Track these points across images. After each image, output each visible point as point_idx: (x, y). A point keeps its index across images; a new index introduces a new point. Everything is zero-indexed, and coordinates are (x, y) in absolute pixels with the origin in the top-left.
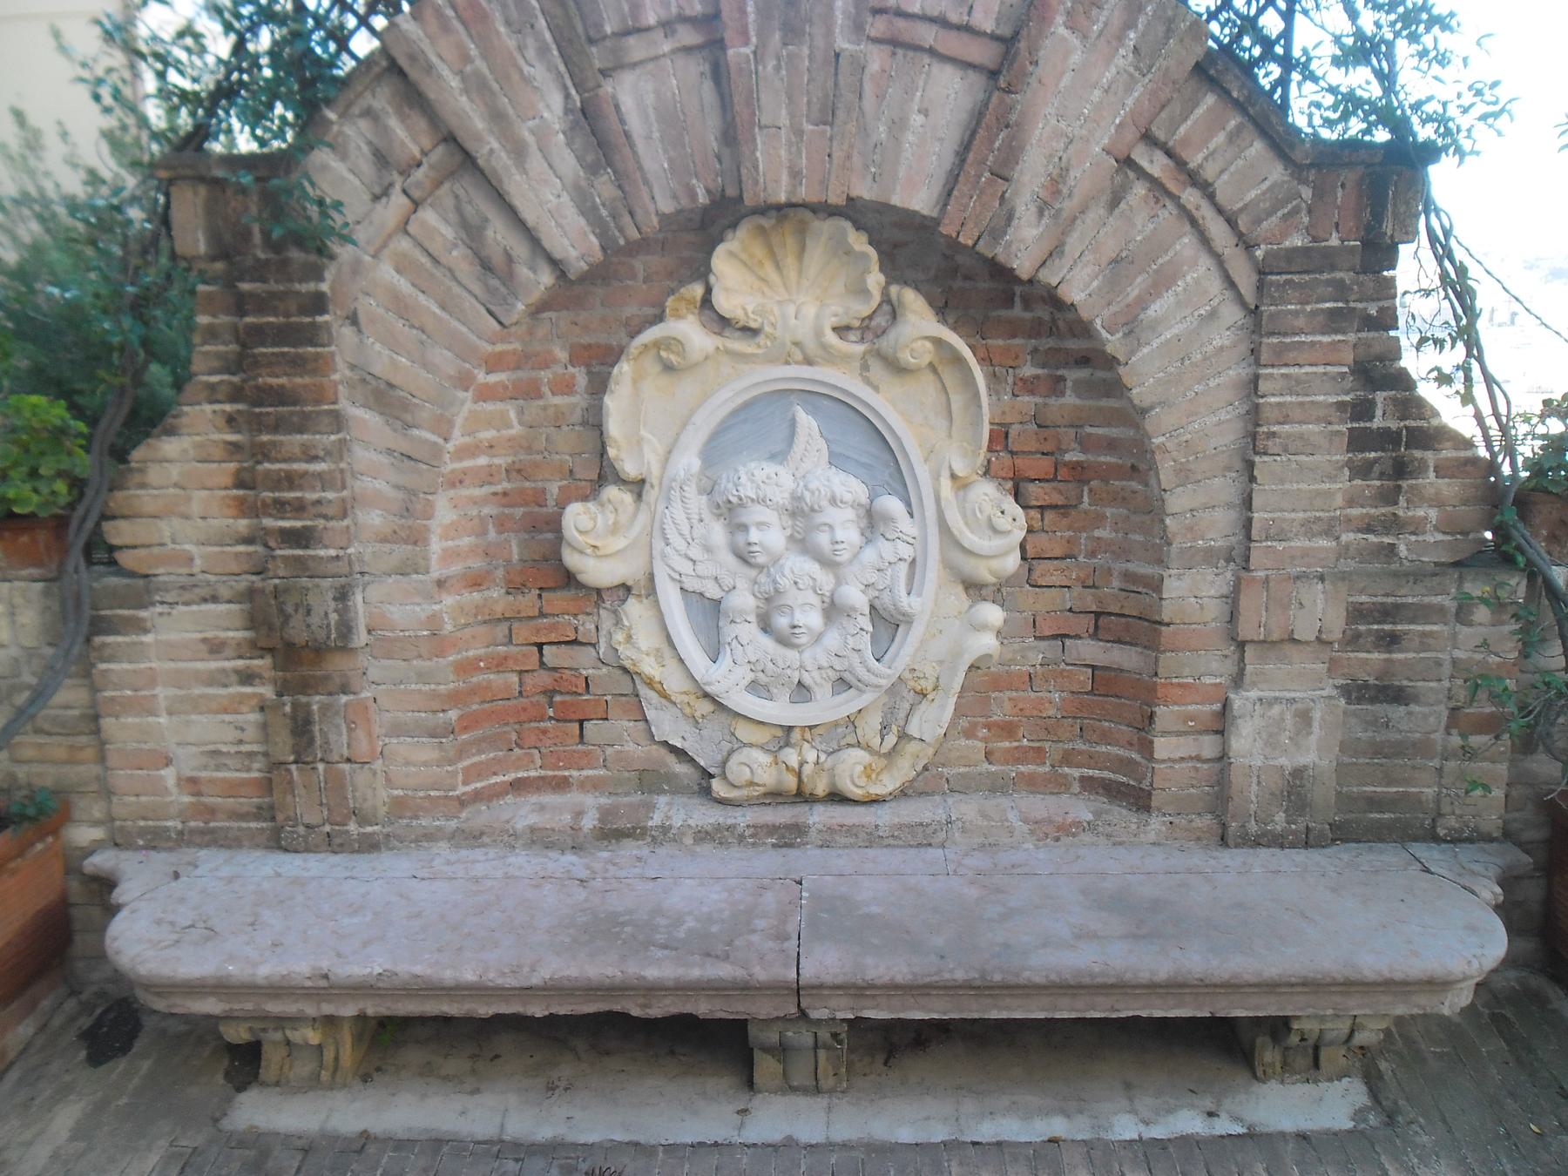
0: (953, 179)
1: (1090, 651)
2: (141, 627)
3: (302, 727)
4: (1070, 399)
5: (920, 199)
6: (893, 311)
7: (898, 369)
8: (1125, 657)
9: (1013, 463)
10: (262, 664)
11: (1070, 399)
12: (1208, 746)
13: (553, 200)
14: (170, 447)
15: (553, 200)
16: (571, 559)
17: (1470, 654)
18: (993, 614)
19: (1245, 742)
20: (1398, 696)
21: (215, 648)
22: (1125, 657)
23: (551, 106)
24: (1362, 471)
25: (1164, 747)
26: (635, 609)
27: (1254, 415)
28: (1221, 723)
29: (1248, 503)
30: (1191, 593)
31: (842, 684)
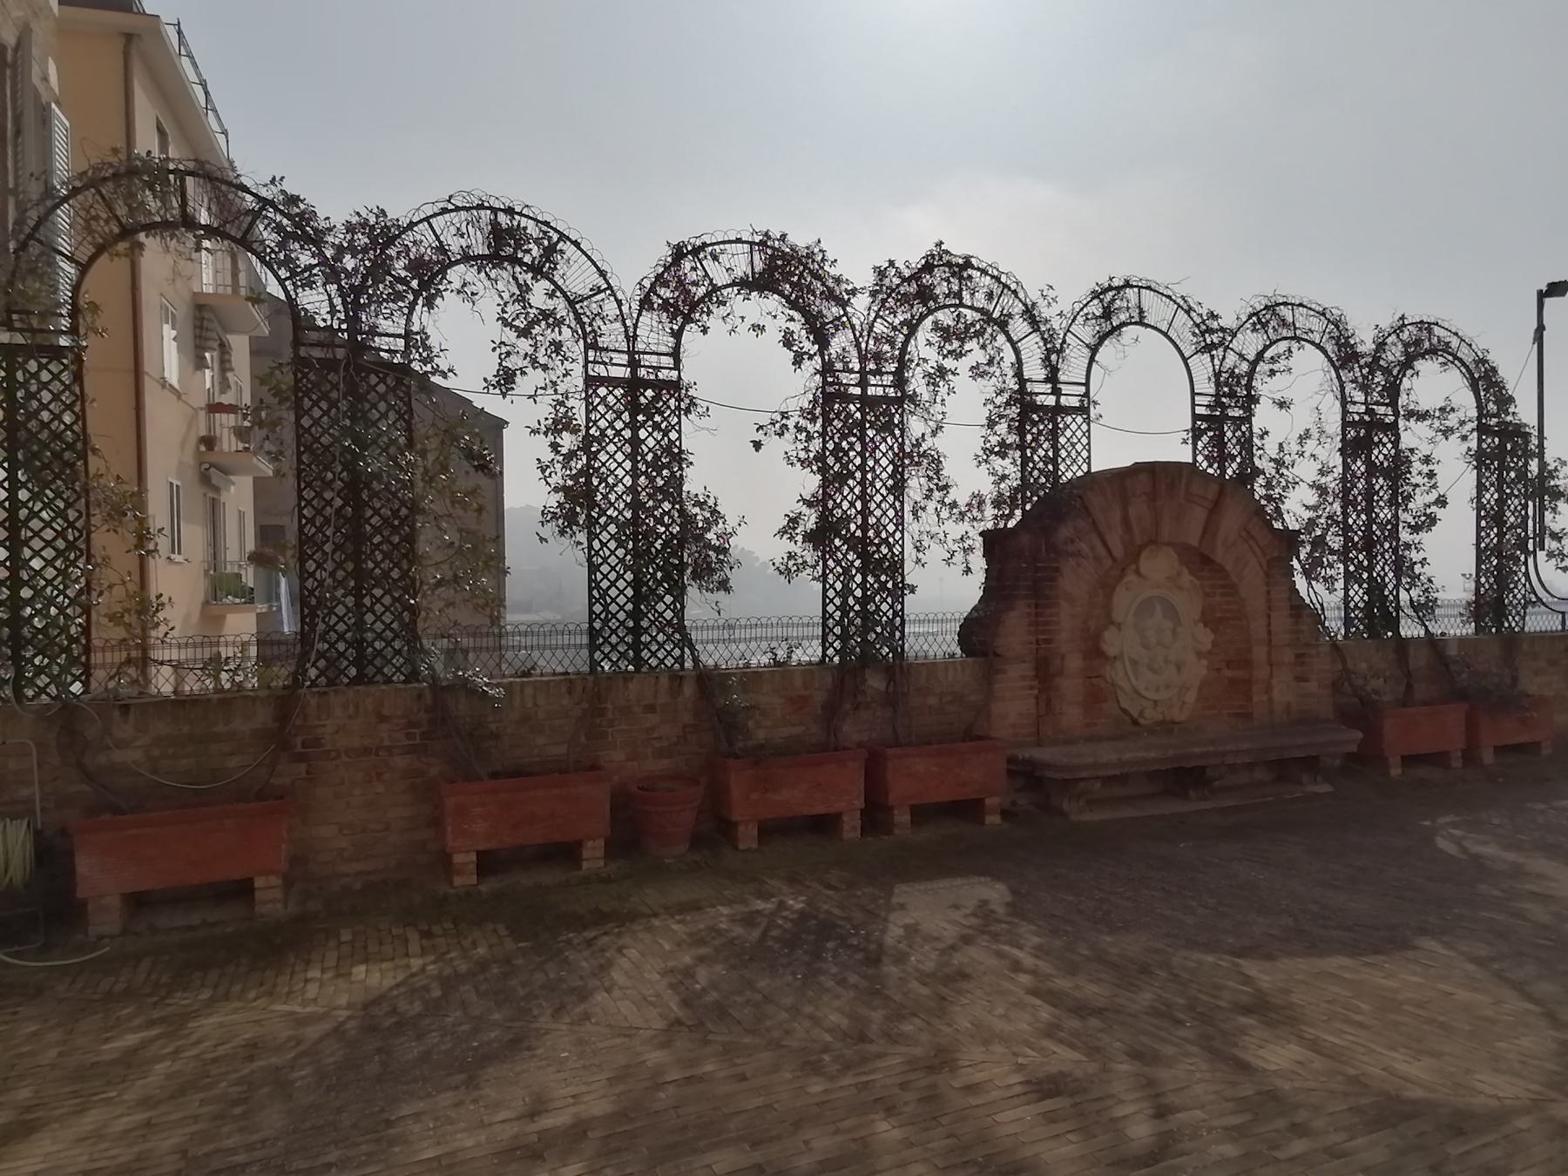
0: (1202, 537)
1: (1229, 673)
2: (1004, 672)
3: (1049, 703)
4: (1218, 598)
5: (1194, 542)
6: (1179, 574)
7: (1180, 588)
8: (1239, 674)
9: (1209, 619)
10: (1035, 683)
11: (1218, 598)
12: (1265, 697)
13: (1116, 541)
14: (1012, 614)
15: (1116, 541)
16: (1104, 647)
17: (515, 1128)
18: (1205, 662)
19: (1276, 694)
20: (1306, 680)
21: (1023, 678)
22: (1239, 674)
23: (1117, 516)
24: (1291, 616)
25: (1255, 699)
26: (1118, 664)
27: (1269, 601)
28: (1269, 689)
29: (1269, 625)
30: (1259, 653)
31: (1167, 687)
